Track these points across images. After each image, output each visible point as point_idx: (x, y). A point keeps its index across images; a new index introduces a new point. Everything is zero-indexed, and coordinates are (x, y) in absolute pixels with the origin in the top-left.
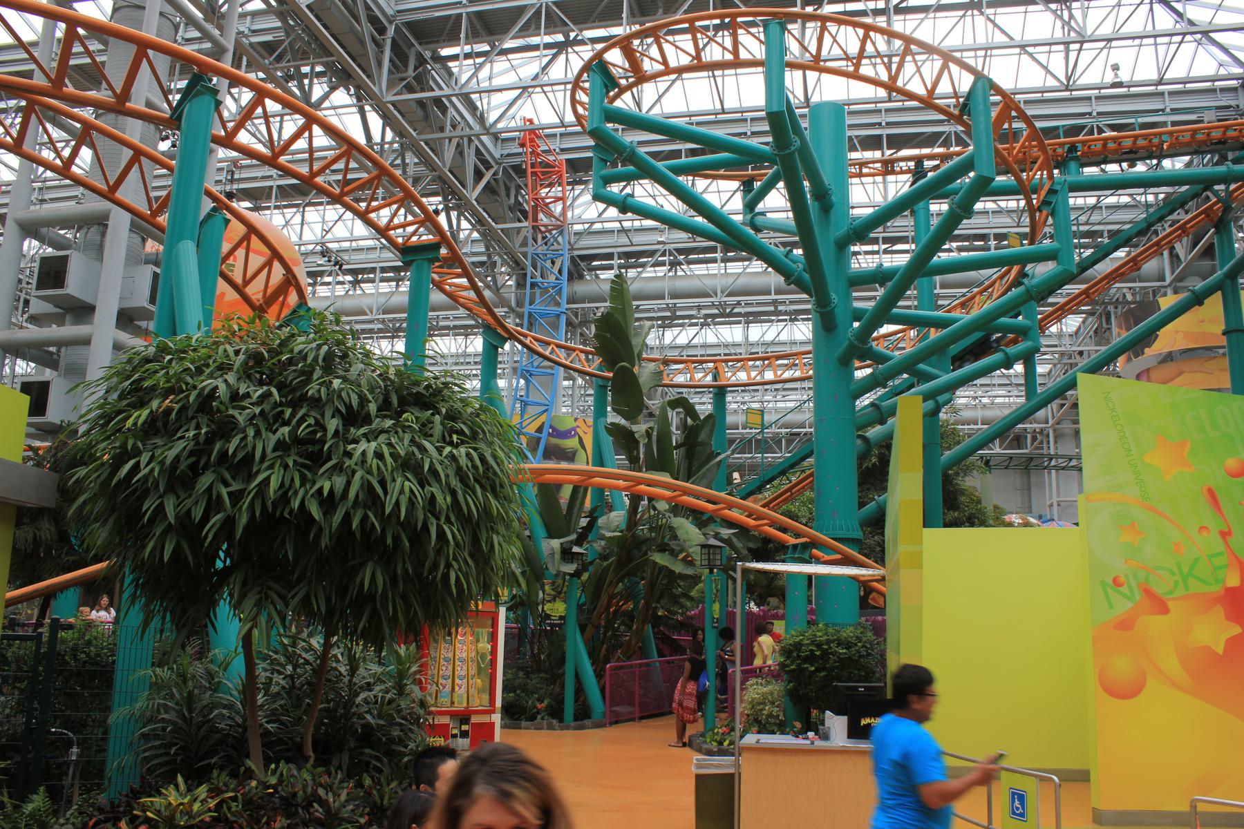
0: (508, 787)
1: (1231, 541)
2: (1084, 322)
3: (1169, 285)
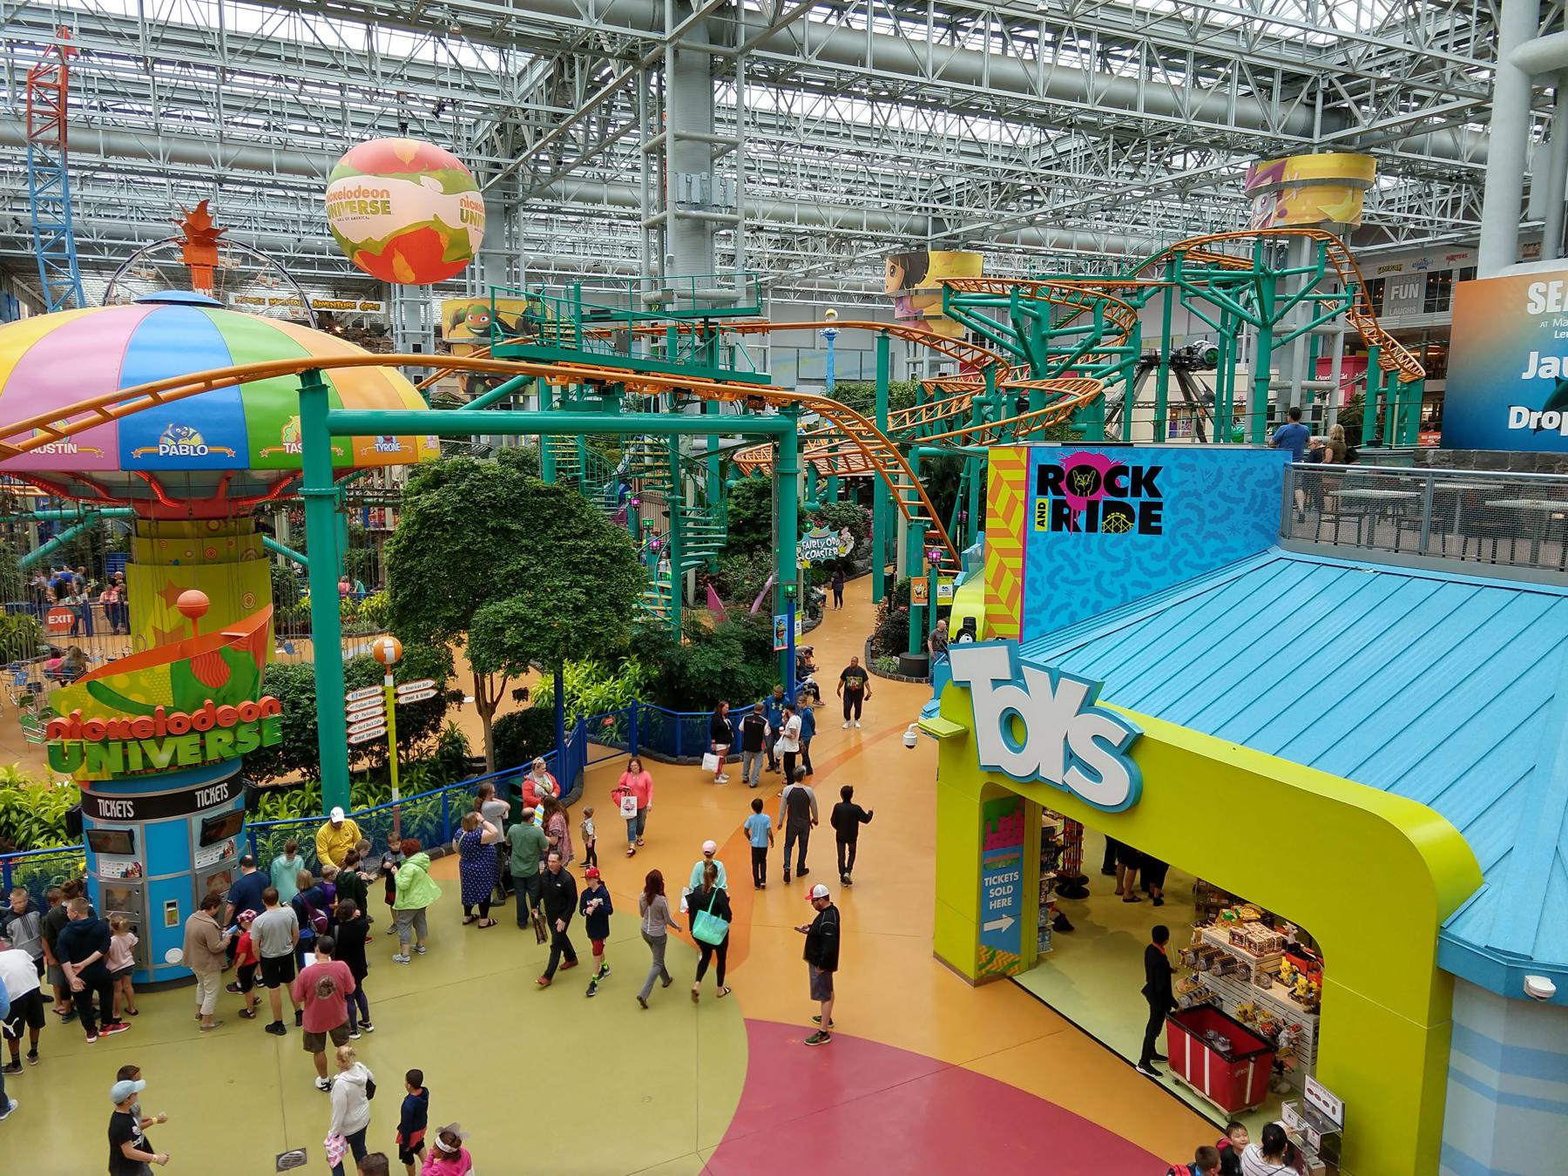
0: (956, 624)
2: (531, 64)
3: (670, 41)
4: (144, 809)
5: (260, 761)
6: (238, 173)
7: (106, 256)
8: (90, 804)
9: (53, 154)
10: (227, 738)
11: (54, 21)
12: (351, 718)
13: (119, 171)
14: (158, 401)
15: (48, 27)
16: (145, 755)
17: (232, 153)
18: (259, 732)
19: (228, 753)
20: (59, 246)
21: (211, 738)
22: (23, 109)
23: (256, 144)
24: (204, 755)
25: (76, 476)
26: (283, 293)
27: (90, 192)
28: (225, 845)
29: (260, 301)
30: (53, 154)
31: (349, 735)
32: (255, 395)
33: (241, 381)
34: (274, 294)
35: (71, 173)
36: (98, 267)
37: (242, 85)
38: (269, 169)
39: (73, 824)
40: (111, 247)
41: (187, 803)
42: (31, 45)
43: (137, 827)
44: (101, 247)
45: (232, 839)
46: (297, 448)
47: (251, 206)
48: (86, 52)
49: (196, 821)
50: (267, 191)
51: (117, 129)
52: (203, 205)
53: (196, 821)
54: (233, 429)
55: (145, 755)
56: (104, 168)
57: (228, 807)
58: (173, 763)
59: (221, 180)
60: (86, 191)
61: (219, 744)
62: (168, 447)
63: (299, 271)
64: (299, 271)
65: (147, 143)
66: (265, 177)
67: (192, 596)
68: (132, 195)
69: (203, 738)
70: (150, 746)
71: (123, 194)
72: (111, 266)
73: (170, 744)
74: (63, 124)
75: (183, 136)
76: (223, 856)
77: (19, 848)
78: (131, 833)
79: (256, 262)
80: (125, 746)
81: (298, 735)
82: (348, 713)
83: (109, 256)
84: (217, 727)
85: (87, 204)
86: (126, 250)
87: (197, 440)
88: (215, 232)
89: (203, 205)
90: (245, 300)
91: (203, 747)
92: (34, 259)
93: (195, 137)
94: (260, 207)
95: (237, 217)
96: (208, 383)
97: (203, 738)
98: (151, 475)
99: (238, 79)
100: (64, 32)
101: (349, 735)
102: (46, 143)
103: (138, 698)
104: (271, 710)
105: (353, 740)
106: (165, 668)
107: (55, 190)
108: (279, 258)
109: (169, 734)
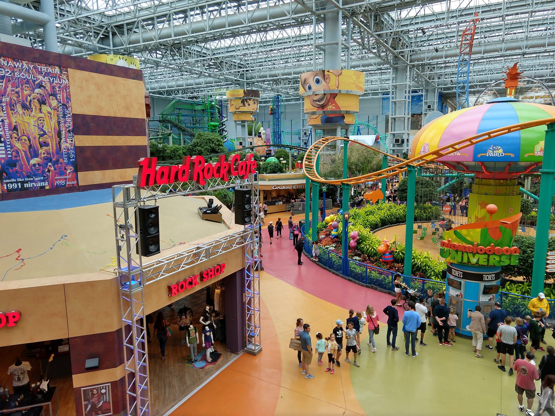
1: (342, 92)
4: (466, 276)
5: (508, 269)
6: (531, 50)
7: (478, 89)
8: (449, 270)
9: (466, 57)
10: (497, 258)
11: (473, 11)
12: (548, 262)
13: (487, 58)
14: (490, 137)
15: (472, 14)
16: (468, 258)
17: (530, 43)
18: (510, 259)
19: (497, 264)
20: (463, 87)
21: (491, 257)
22: (459, 44)
23: (540, 38)
24: (488, 263)
25: (458, 163)
26: (542, 94)
27: (477, 68)
28: (491, 296)
29: (532, 98)
30: (466, 57)
31: (547, 268)
32: (525, 134)
33: (522, 128)
34: (537, 94)
35: (471, 62)
36: (474, 93)
37: (539, 16)
38: (544, 45)
39: (444, 275)
40: (479, 85)
41: (479, 278)
42: (465, 22)
43: (463, 281)
44: (476, 86)
45: (494, 295)
46: (541, 154)
47: (534, 61)
48: (482, 19)
49: (482, 285)
50: (541, 54)
51: (490, 43)
52: (516, 64)
53: (482, 285)
54: (516, 147)
55: (468, 258)
56: (482, 58)
57: (494, 283)
58: (477, 263)
59: (524, 54)
60: (475, 67)
61: (494, 260)
62: (490, 153)
63: (550, 84)
64: (550, 84)
65: (498, 46)
66: (542, 49)
67: (492, 206)
68: (490, 66)
69: (488, 256)
70: (471, 255)
71: (487, 66)
72: (480, 92)
73: (477, 256)
74: (471, 45)
75: (512, 41)
76: (490, 300)
77: (428, 278)
78: (460, 282)
79: (532, 82)
80: (463, 254)
81: (524, 263)
82: (548, 260)
83: (477, 89)
84: (494, 254)
85: (475, 72)
86: (485, 86)
87: (501, 151)
88: (518, 74)
89: (516, 64)
90: (526, 98)
91: (488, 260)
92: (455, 93)
93: (517, 40)
94: (538, 61)
95: (527, 67)
96: (509, 130)
97: (488, 256)
98: (482, 163)
99: (538, 14)
100: (476, 14)
101: (547, 268)
102: (464, 54)
103: (469, 238)
104: (516, 252)
105: (548, 271)
106: (479, 230)
107: (465, 69)
108: (542, 80)
109: (477, 253)
